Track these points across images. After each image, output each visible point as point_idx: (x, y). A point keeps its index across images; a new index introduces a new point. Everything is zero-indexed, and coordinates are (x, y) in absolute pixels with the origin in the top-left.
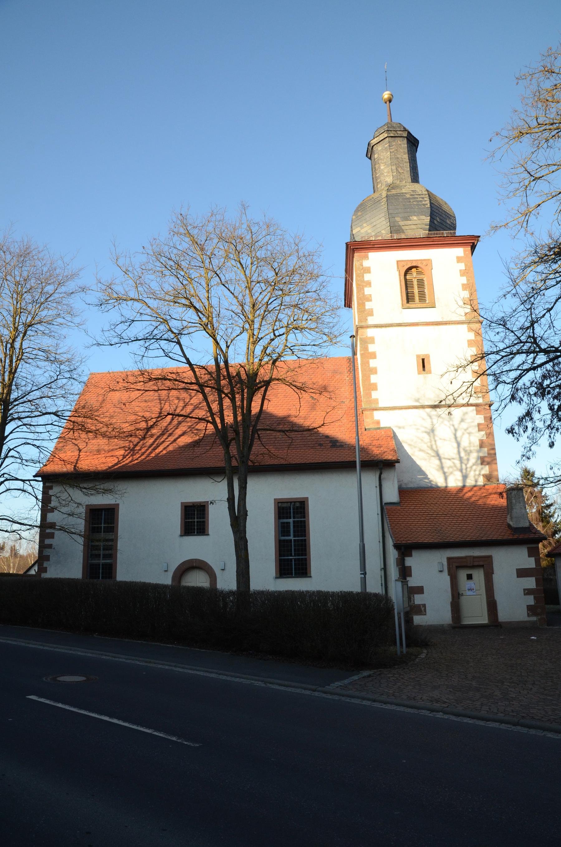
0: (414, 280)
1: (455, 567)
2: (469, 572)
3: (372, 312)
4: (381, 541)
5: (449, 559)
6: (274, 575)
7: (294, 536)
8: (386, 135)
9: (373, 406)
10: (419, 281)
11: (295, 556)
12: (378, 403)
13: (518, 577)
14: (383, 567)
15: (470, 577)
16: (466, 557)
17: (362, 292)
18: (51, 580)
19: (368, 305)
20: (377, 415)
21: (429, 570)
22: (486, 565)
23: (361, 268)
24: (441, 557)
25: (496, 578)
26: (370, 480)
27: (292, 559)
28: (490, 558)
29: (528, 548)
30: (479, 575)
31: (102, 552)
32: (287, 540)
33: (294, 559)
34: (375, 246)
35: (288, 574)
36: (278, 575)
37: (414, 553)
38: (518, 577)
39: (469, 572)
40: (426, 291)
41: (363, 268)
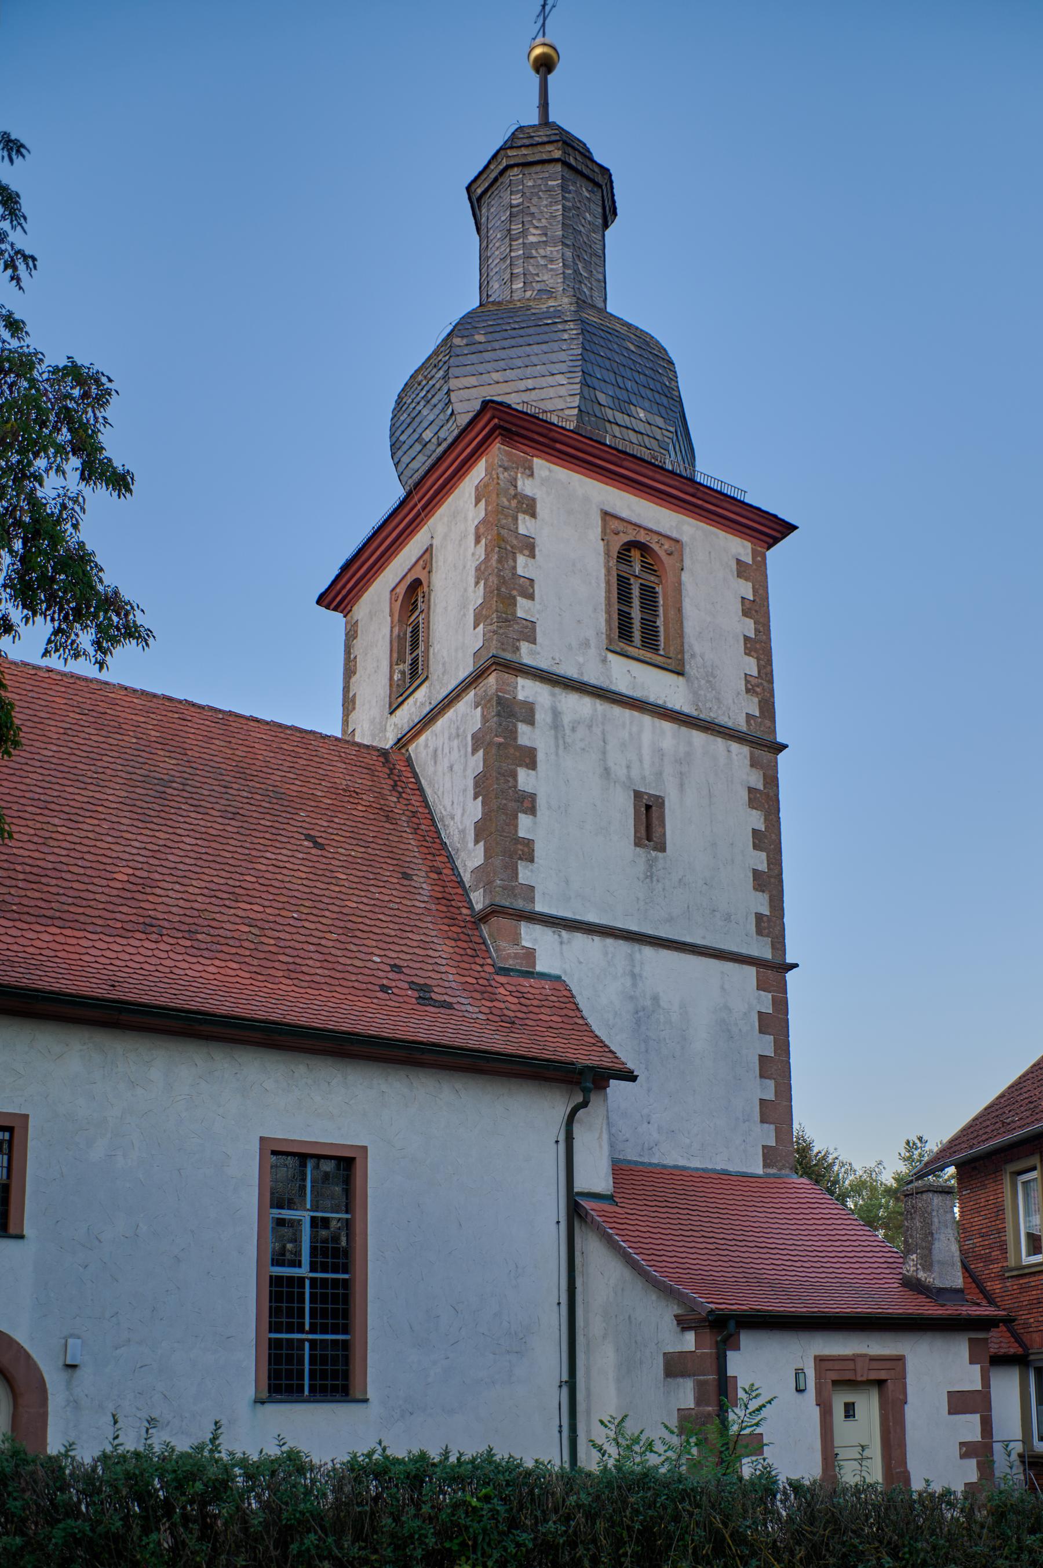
0: (632, 581)
1: (839, 1379)
2: (850, 1398)
3: (534, 630)
4: (564, 1300)
5: (820, 1361)
6: (251, 1392)
7: (313, 1268)
8: (557, 154)
9: (520, 904)
10: (644, 588)
11: (313, 1331)
12: (532, 900)
13: (950, 1413)
14: (565, 1377)
15: (850, 1411)
16: (853, 1359)
17: (511, 562)
18: (883, 1479)
19: (523, 608)
20: (532, 936)
21: (778, 1394)
22: (886, 1383)
23: (513, 492)
24: (804, 1352)
25: (912, 1413)
26: (540, 1113)
27: (303, 1341)
28: (900, 1359)
29: (970, 1340)
30: (868, 1406)
31: (341, 1291)
32: (291, 1279)
33: (311, 1341)
34: (558, 446)
35: (335, 1389)
36: (265, 1394)
37: (746, 1339)
38: (950, 1413)
39: (850, 1398)
40: (660, 622)
41: (515, 496)
